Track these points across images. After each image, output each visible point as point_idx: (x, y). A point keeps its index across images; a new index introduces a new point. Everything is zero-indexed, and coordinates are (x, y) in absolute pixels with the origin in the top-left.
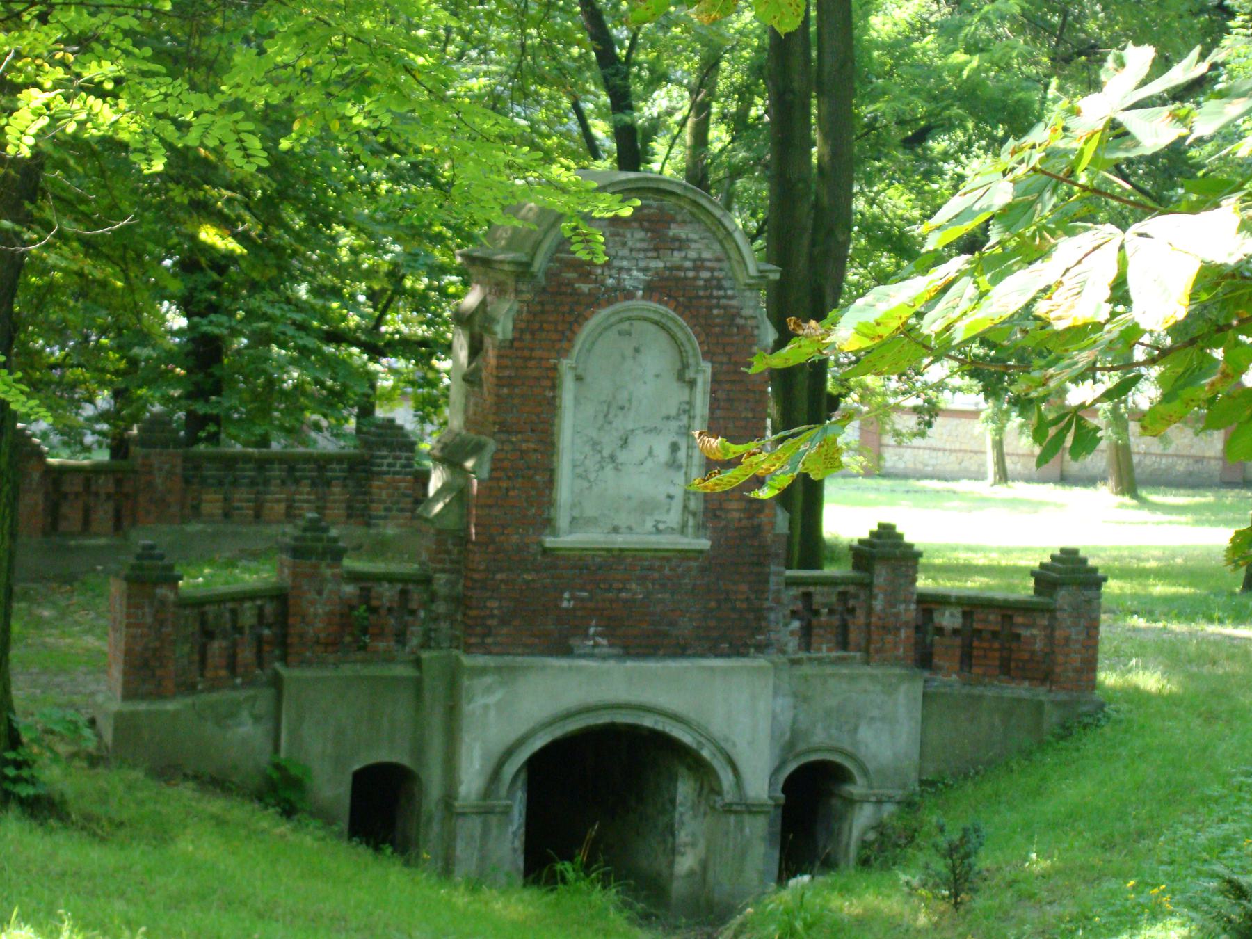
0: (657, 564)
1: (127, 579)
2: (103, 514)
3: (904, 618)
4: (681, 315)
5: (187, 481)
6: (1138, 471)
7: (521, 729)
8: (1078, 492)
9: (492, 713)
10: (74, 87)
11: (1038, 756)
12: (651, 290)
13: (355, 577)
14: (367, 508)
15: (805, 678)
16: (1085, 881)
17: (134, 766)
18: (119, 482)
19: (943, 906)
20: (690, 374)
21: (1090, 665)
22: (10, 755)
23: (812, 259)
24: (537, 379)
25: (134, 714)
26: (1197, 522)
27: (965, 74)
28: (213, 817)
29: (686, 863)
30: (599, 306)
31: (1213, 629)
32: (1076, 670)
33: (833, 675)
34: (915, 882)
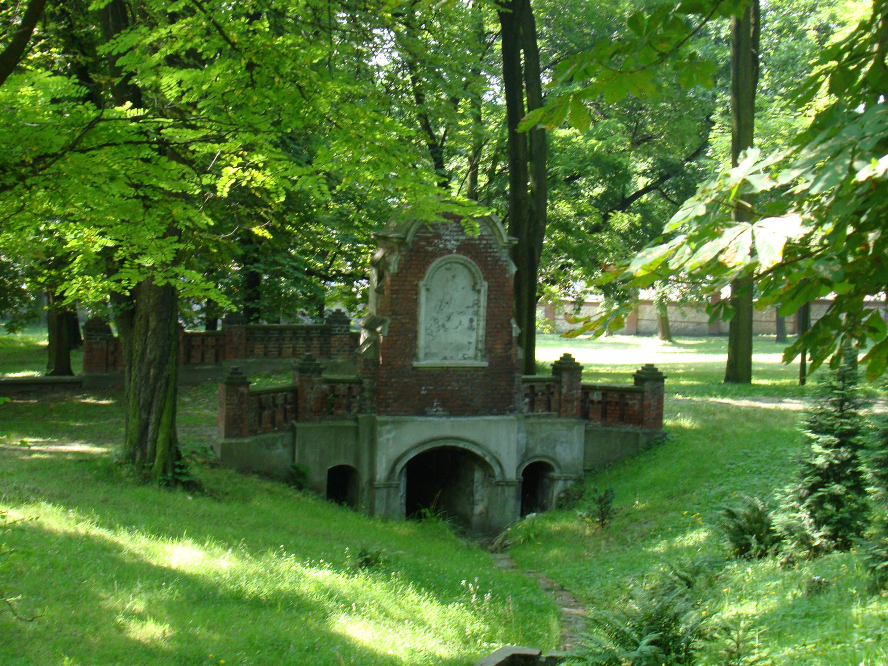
1: (226, 383)
2: (210, 354)
3: (576, 396)
4: (474, 260)
5: (248, 339)
6: (671, 329)
7: (404, 449)
8: (644, 340)
9: (391, 442)
10: (244, 166)
11: (637, 458)
12: (460, 249)
13: (327, 381)
15: (532, 424)
16: (660, 513)
17: (230, 468)
18: (217, 340)
19: (596, 526)
20: (478, 287)
21: (659, 417)
22: (177, 463)
25: (230, 444)
26: (698, 352)
27: (595, 149)
28: (267, 490)
29: (479, 508)
31: (712, 399)
34: (584, 515)
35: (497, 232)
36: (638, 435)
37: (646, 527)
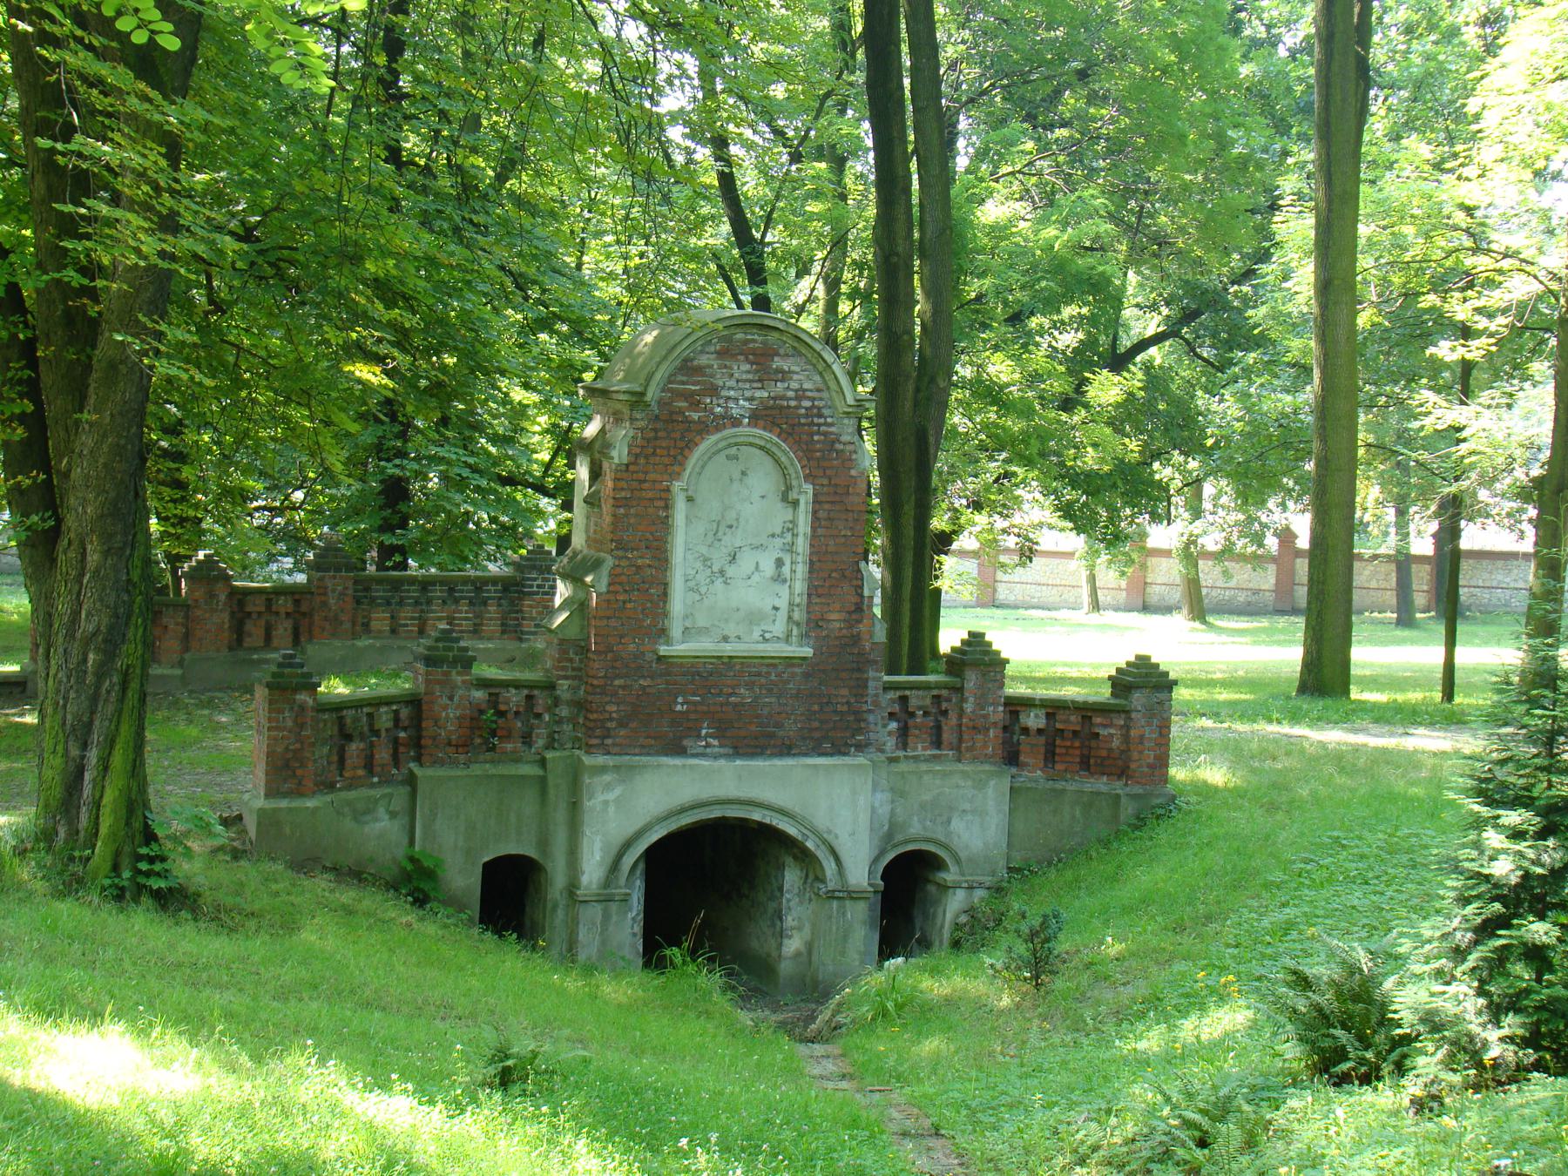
0: (764, 670)
1: (268, 685)
2: (283, 629)
9: (611, 809)
12: (755, 418)
13: (484, 683)
14: (519, 625)
15: (902, 774)
16: (1157, 963)
18: (297, 602)
19: (1026, 987)
20: (793, 495)
21: (1162, 762)
23: (916, 404)
24: (651, 500)
25: (274, 810)
29: (793, 945)
30: (708, 433)
31: (1273, 728)
32: (1150, 766)
33: (927, 772)
34: (999, 966)
35: (833, 385)
36: (1118, 796)
37: (1126, 993)
